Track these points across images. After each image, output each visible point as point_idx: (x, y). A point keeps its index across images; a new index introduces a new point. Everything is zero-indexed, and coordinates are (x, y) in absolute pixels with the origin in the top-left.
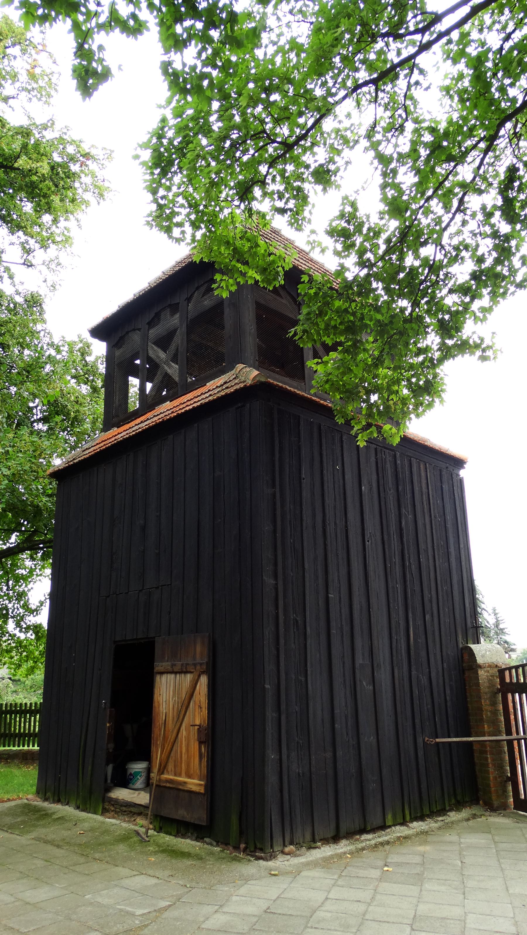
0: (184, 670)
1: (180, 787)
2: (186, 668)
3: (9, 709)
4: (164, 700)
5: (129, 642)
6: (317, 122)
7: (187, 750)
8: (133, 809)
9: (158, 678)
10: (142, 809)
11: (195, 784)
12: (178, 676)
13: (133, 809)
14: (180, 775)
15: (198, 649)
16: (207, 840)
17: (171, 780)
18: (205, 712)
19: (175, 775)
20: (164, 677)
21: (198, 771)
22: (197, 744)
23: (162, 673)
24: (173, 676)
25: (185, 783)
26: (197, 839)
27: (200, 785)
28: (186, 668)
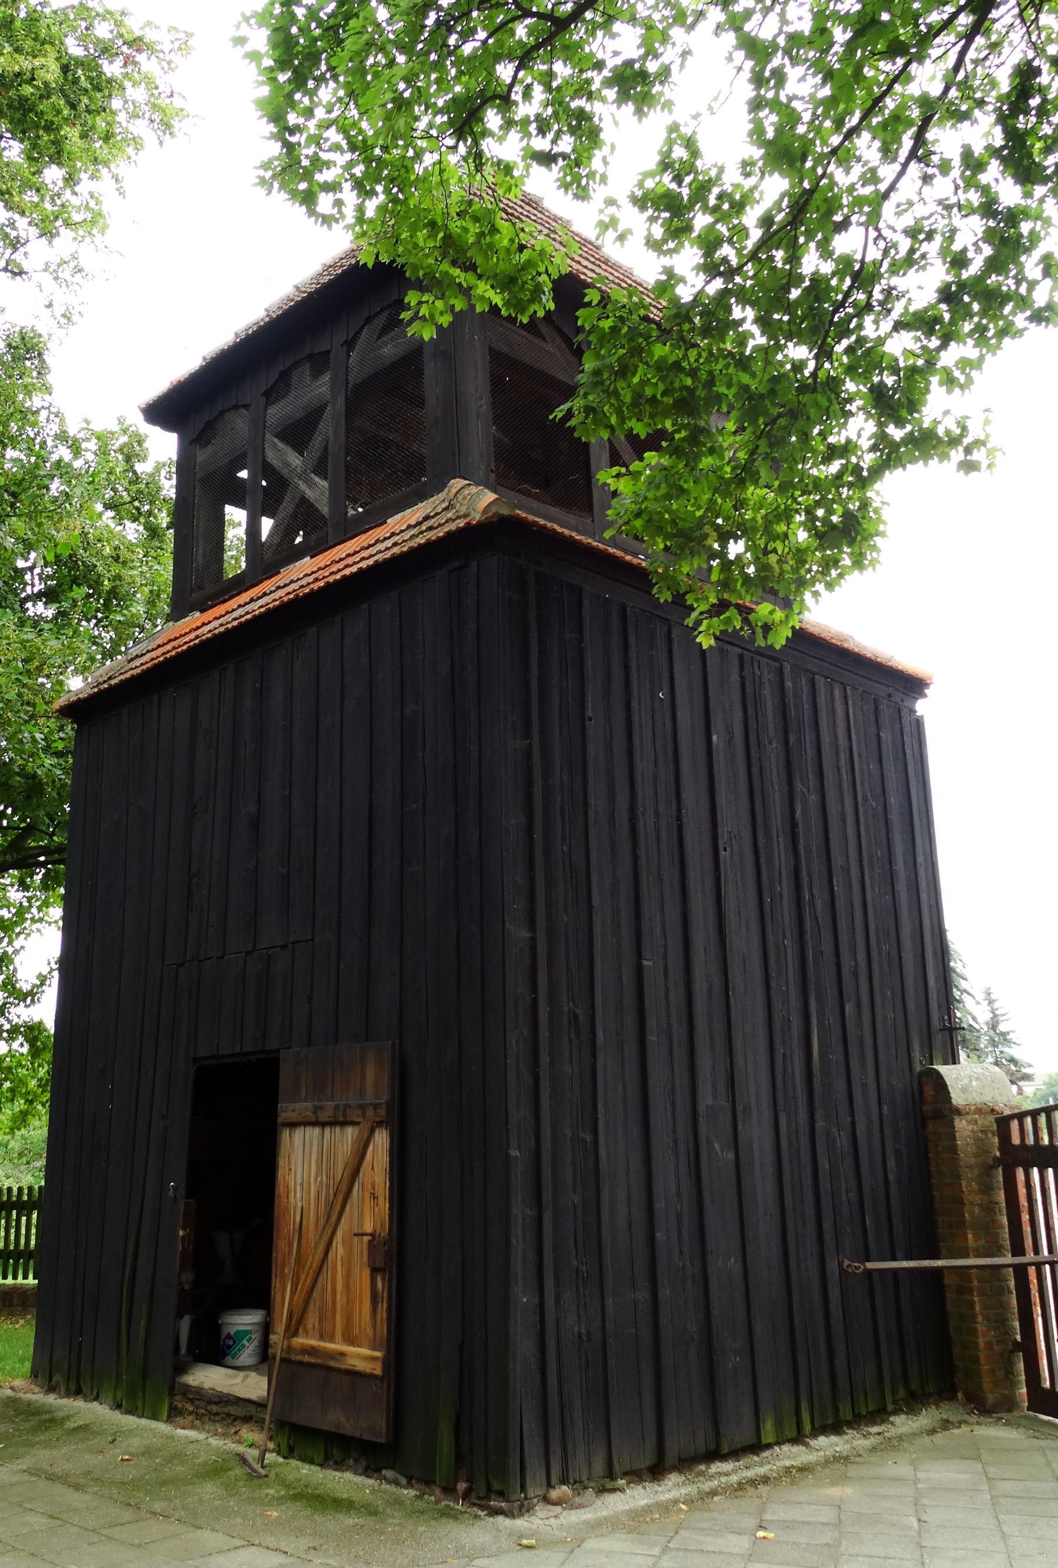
0: (341, 1118)
1: (332, 1364)
2: (344, 1115)
4: (299, 1181)
7: (347, 1286)
8: (232, 1410)
9: (285, 1134)
11: (363, 1357)
14: (332, 1339)
15: (370, 1074)
16: (388, 1473)
19: (322, 1338)
20: (299, 1134)
21: (369, 1331)
22: (367, 1272)
23: (293, 1125)
24: (317, 1131)
25: (342, 1354)
26: (367, 1472)
27: (374, 1359)
28: (344, 1115)
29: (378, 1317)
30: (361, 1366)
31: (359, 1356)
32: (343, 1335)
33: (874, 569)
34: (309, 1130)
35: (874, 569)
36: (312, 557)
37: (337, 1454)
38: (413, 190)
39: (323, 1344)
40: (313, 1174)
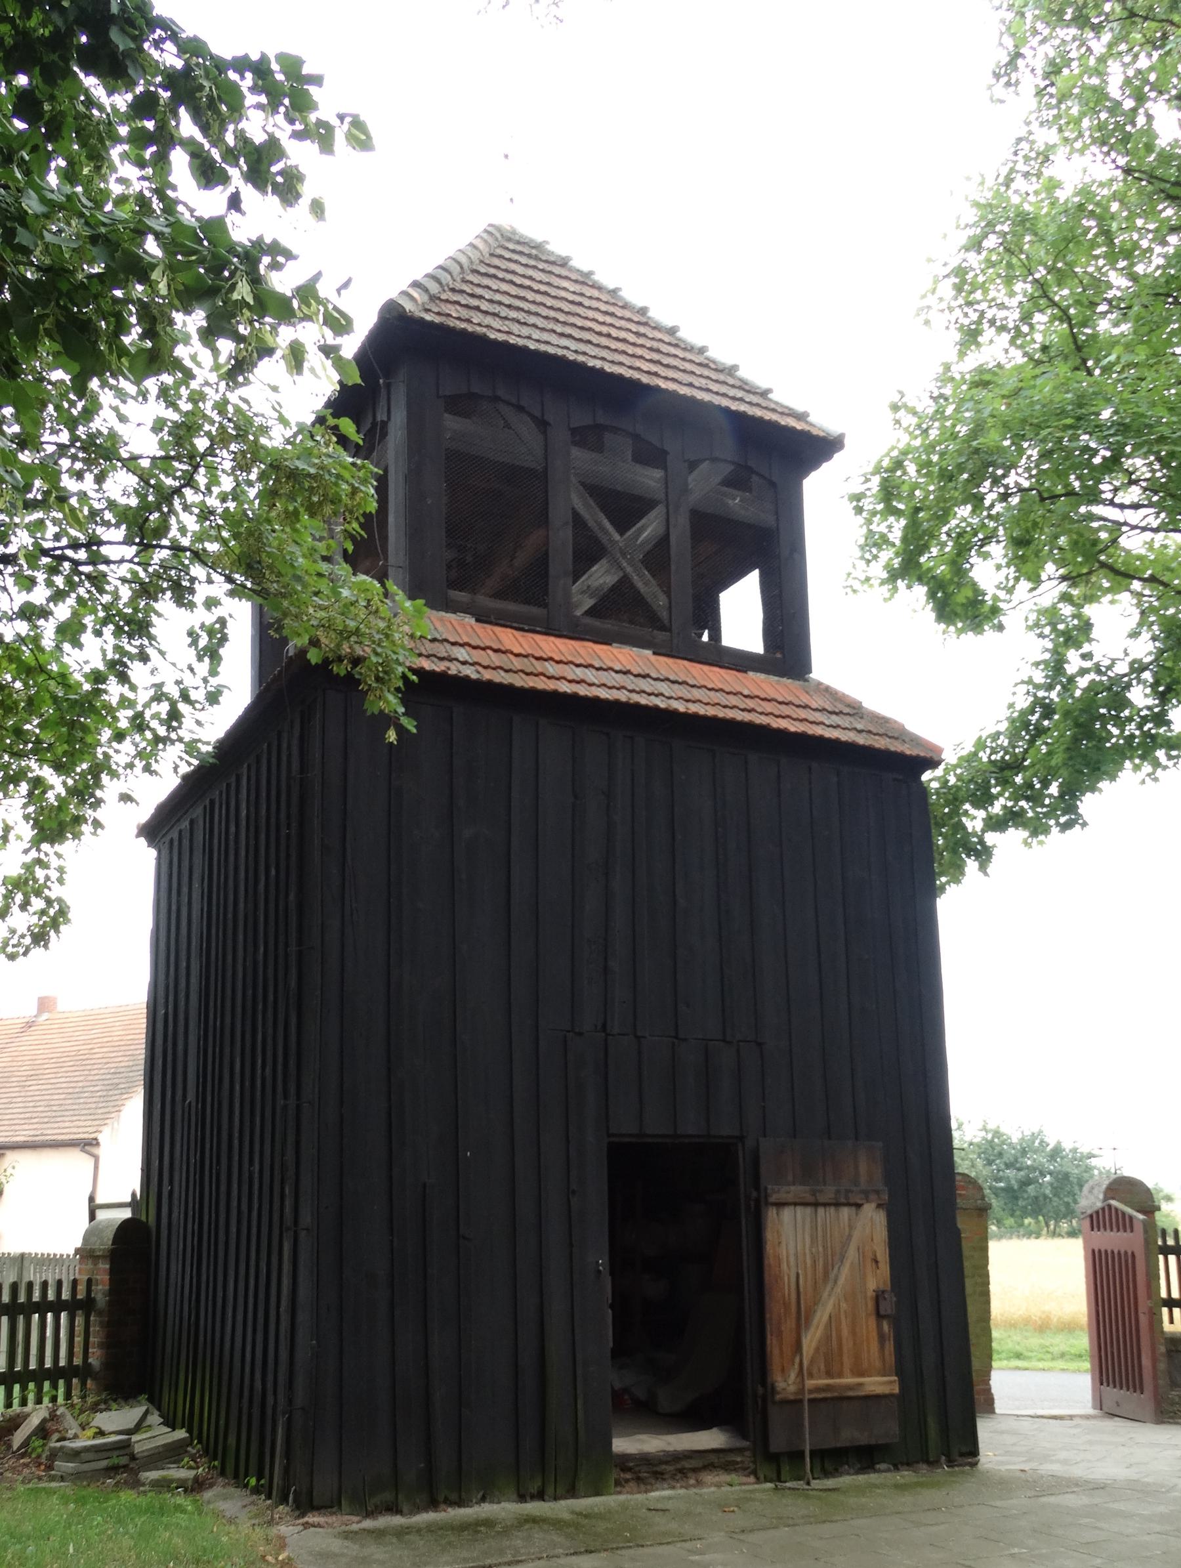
0: (843, 1200)
1: (851, 1394)
2: (847, 1197)
3: (80, 1296)
4: (792, 1252)
5: (650, 1140)
6: (1090, 573)
7: (853, 1333)
8: (687, 1464)
9: (772, 1213)
10: (713, 1458)
11: (880, 1384)
12: (821, 1210)
13: (687, 1464)
14: (840, 1375)
15: (863, 1168)
16: (883, 1466)
17: (828, 1385)
18: (885, 1268)
19: (829, 1374)
20: (787, 1213)
23: (780, 1205)
25: (861, 1385)
26: (862, 1470)
27: (891, 1382)
28: (847, 1197)
29: (887, 1352)
30: (880, 1390)
31: (874, 1383)
32: (851, 1371)
33: (317, 80)
34: (799, 1209)
35: (317, 80)
36: (654, 653)
37: (829, 1466)
38: (1108, 745)
39: (838, 1381)
40: (807, 1246)
